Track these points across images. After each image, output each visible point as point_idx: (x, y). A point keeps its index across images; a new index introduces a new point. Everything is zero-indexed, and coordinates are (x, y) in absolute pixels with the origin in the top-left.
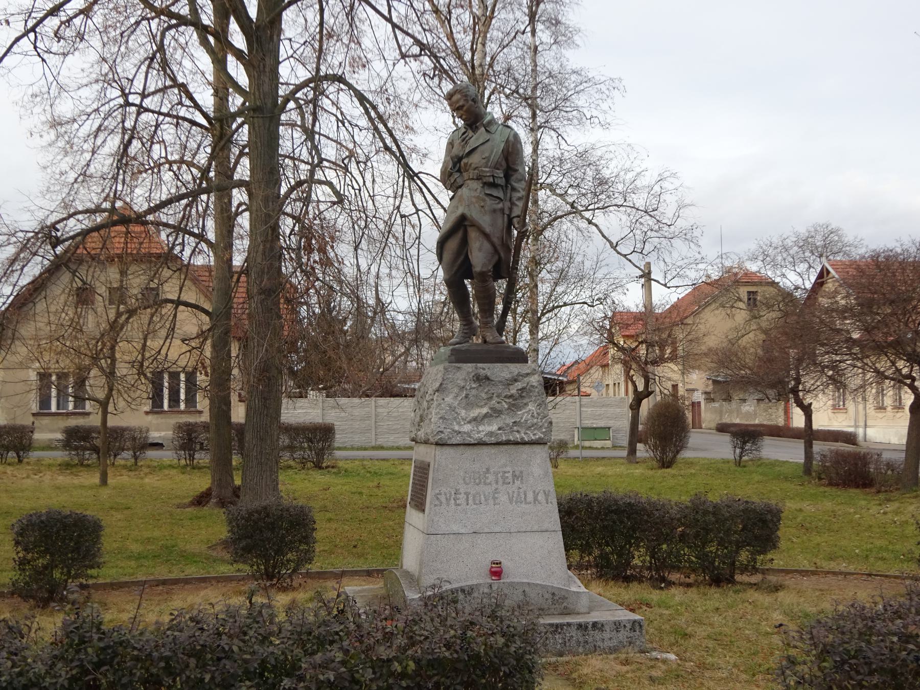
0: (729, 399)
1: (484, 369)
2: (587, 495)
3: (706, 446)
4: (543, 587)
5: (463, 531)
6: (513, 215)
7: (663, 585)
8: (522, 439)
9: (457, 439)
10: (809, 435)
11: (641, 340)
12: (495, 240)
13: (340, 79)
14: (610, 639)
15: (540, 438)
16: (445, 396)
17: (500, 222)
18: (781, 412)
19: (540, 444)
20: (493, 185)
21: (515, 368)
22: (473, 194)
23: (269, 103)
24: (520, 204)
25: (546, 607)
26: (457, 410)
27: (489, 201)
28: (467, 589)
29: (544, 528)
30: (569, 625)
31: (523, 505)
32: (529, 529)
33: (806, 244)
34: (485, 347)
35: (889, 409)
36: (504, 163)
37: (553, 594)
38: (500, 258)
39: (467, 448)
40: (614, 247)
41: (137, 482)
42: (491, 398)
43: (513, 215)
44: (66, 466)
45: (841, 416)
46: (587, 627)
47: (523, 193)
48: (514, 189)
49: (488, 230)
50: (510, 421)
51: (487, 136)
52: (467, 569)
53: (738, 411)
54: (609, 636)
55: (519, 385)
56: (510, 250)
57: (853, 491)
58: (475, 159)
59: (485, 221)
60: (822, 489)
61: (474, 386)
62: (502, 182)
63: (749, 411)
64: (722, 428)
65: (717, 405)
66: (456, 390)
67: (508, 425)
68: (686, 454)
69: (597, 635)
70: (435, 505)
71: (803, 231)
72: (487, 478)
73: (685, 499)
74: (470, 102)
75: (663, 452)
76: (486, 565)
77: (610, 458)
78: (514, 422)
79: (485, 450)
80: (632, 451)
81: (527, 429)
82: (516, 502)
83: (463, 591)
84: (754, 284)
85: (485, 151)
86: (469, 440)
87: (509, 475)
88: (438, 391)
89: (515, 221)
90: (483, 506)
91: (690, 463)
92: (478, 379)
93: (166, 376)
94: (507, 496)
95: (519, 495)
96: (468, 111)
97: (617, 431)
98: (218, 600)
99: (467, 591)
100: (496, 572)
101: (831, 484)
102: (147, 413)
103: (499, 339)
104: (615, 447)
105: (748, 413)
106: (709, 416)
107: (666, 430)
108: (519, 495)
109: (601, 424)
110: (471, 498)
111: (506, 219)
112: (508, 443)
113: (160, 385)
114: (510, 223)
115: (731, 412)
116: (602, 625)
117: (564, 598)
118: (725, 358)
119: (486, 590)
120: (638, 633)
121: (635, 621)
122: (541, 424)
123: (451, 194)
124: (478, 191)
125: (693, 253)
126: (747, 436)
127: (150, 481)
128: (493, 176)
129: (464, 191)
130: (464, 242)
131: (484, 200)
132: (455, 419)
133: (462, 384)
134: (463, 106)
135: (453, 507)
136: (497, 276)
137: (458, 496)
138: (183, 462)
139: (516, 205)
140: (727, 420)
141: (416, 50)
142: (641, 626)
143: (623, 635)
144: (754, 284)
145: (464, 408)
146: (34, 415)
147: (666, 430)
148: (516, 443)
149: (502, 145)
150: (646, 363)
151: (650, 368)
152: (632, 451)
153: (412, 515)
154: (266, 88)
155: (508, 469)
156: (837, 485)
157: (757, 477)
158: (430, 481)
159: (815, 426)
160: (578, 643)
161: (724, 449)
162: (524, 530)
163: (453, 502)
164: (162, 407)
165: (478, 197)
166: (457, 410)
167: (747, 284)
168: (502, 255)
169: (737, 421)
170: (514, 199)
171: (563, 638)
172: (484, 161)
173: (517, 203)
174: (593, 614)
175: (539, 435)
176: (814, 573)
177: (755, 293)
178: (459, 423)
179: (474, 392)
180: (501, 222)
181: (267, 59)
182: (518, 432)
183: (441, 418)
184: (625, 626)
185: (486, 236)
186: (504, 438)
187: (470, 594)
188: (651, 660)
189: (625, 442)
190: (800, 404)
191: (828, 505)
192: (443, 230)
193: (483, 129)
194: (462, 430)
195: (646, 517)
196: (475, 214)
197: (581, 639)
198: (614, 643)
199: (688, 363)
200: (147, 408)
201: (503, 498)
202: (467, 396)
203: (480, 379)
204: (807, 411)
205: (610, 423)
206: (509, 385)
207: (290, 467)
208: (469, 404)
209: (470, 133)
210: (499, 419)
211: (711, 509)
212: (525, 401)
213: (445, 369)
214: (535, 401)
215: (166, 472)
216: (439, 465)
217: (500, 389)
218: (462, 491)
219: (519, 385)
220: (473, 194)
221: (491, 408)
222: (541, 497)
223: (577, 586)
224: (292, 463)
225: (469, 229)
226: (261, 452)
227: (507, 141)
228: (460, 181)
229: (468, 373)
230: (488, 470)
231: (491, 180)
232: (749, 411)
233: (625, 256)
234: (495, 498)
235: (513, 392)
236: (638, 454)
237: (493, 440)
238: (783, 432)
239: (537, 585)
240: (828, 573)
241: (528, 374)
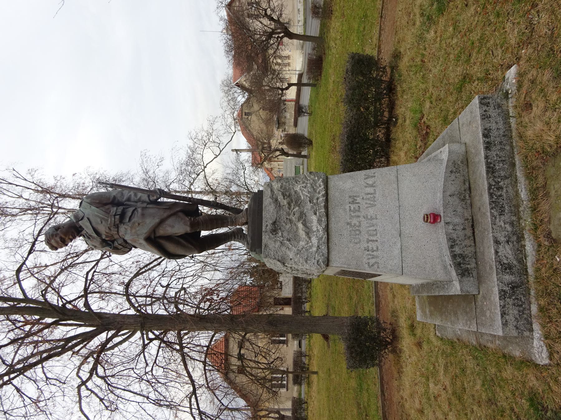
0: (284, 123)
1: (267, 226)
2: (342, 163)
3: (304, 127)
4: (446, 180)
5: (399, 246)
6: (147, 200)
7: (394, 119)
8: (323, 196)
9: (324, 248)
10: (299, 85)
11: (262, 153)
12: (165, 215)
14: (497, 123)
15: (323, 182)
17: (151, 211)
18: (290, 103)
19: (327, 181)
20: (122, 216)
21: (267, 201)
22: (129, 231)
23: (139, 319)
24: (139, 195)
25: (462, 178)
26: (300, 248)
27: (135, 219)
28: (450, 243)
29: (395, 179)
30: (486, 157)
31: (377, 195)
32: (396, 191)
33: (227, 93)
34: (250, 223)
35: (289, 61)
36: (107, 207)
37: (451, 172)
38: (180, 211)
39: (330, 240)
40: (217, 156)
41: (316, 358)
42: (290, 220)
43: (147, 200)
44: (309, 384)
46: (488, 143)
47: (132, 193)
48: (129, 199)
49: (157, 220)
50: (309, 205)
51: (85, 219)
52: (431, 242)
53: (289, 119)
54: (494, 124)
55: (280, 198)
56: (176, 202)
57: (324, 64)
58: (102, 229)
59: (150, 223)
60: (323, 78)
61: (280, 234)
62: (120, 209)
63: (290, 115)
65: (287, 127)
66: (283, 249)
67: (312, 207)
68: (306, 135)
69: (494, 133)
70: (378, 267)
71: (223, 94)
72: (355, 224)
73: (342, 108)
74: (58, 232)
75: (305, 144)
76: (427, 227)
77: (308, 166)
78: (310, 202)
79: (332, 226)
80: (305, 157)
81: (316, 192)
82: (375, 201)
83: (452, 247)
84: (242, 113)
85: (96, 222)
86: (324, 239)
88: (284, 264)
90: (378, 228)
91: (310, 133)
94: (370, 209)
95: (369, 199)
96: (66, 234)
97: (296, 163)
99: (452, 243)
100: (433, 218)
101: (320, 75)
102: (287, 346)
103: (244, 212)
104: (303, 164)
105: (290, 116)
107: (297, 142)
108: (369, 199)
109: (294, 169)
110: (372, 238)
111: (150, 206)
112: (326, 207)
114: (155, 202)
115: (289, 122)
116: (486, 129)
117: (454, 163)
118: (268, 122)
119: (451, 227)
120: (490, 100)
121: (481, 103)
122: (311, 181)
123: (133, 248)
124: (126, 227)
125: (220, 120)
126: (299, 111)
127: (316, 351)
128: (115, 215)
129: (128, 238)
130: (169, 238)
131: (134, 223)
132: (307, 250)
133: (278, 244)
134: (61, 238)
135: (379, 252)
137: (370, 248)
138: (308, 337)
139: (140, 197)
140: (292, 124)
142: (485, 98)
143: (492, 112)
144: (242, 113)
145: (298, 242)
146: (287, 390)
147: (297, 142)
148: (327, 201)
149: (93, 208)
152: (305, 157)
154: (132, 321)
155: (347, 207)
156: (321, 72)
157: (317, 105)
158: (357, 271)
159: (296, 82)
160: (502, 149)
161: (304, 121)
162: (397, 196)
163: (375, 253)
164: (285, 340)
165: (131, 228)
166: (300, 248)
167: (242, 115)
168: (178, 209)
169: (293, 120)
170: (136, 199)
171: (498, 163)
172: (104, 222)
173: (138, 197)
175: (320, 182)
176: (379, 47)
177: (245, 113)
178: (311, 247)
179: (285, 234)
180: (152, 210)
181: (118, 320)
182: (318, 199)
183: (306, 262)
184: (485, 111)
185: (162, 222)
186: (323, 210)
187: (454, 241)
188: (520, 86)
191: (331, 71)
193: (80, 222)
194: (316, 245)
195: (355, 129)
196: (145, 230)
197: (499, 147)
198: (500, 119)
199: (270, 136)
200: (285, 346)
201: (371, 212)
205: (294, 166)
206: (280, 206)
207: (310, 293)
208: (295, 238)
209: (83, 232)
210: (307, 214)
211: (351, 91)
212: (293, 193)
213: (266, 257)
214: (293, 185)
215: (311, 344)
216: (345, 264)
217: (283, 213)
218: (366, 245)
219: (280, 198)
220: (129, 231)
221: (299, 221)
224: (308, 293)
225: (158, 235)
226: (309, 325)
227: (91, 204)
228: (120, 241)
229: (270, 238)
230: (348, 224)
231: (118, 217)
232: (290, 115)
233: (221, 151)
234: (372, 219)
235: (285, 202)
236: (306, 154)
239: (445, 185)
240: (379, 40)
241: (272, 191)
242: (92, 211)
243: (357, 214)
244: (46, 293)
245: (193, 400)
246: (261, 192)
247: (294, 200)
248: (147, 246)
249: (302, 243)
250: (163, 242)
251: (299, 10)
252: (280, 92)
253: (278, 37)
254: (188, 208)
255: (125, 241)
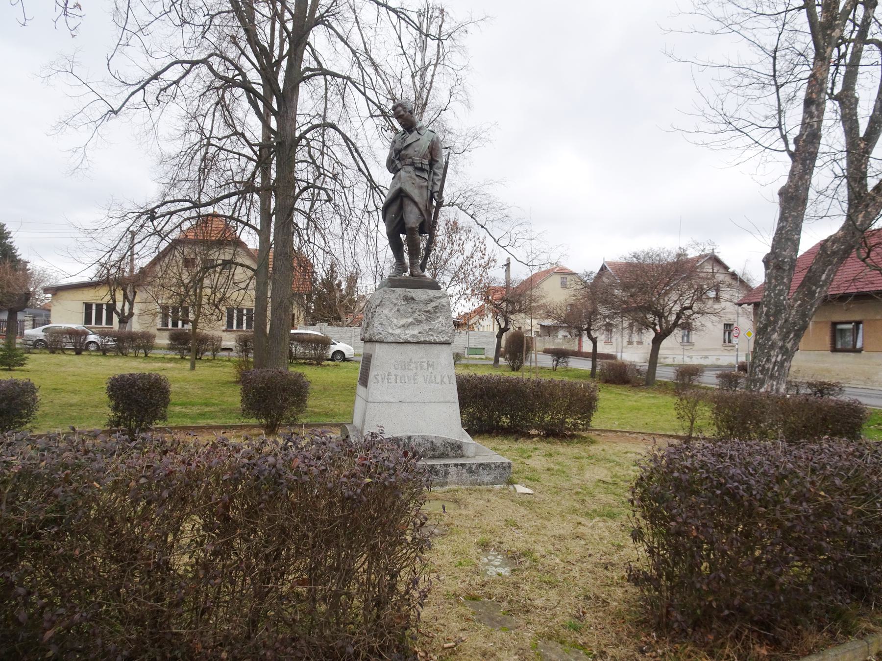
5: (392, 400)
9: (391, 339)
10: (594, 356)
12: (421, 206)
13: (333, 126)
16: (391, 321)
18: (577, 343)
20: (422, 170)
21: (432, 293)
24: (439, 183)
35: (635, 343)
36: (429, 155)
45: (608, 346)
47: (441, 177)
48: (435, 174)
50: (427, 328)
51: (419, 137)
55: (434, 304)
58: (410, 151)
59: (415, 193)
62: (427, 168)
64: (546, 351)
75: (514, 362)
79: (409, 347)
80: (496, 360)
86: (399, 340)
87: (425, 364)
89: (435, 194)
92: (406, 299)
93: (235, 311)
98: (245, 440)
106: (540, 344)
107: (516, 348)
110: (398, 378)
112: (425, 342)
113: (234, 316)
114: (432, 197)
123: (393, 175)
126: (560, 354)
129: (402, 173)
130: (401, 208)
133: (395, 301)
136: (422, 231)
141: (378, 112)
149: (429, 143)
150: (507, 312)
151: (508, 315)
152: (496, 360)
153: (360, 389)
155: (424, 360)
161: (547, 361)
174: (477, 457)
175: (446, 338)
178: (392, 328)
179: (403, 307)
180: (426, 194)
189: (493, 356)
190: (590, 337)
192: (388, 198)
200: (224, 328)
201: (420, 379)
202: (398, 310)
203: (408, 299)
204: (594, 341)
218: (393, 374)
219: (434, 304)
222: (446, 380)
223: (467, 439)
227: (432, 141)
232: (561, 340)
237: (415, 340)
238: (578, 354)
241: (440, 297)
242: (425, 142)
243: (419, 368)
244: (325, 25)
245: (188, 205)
246: (439, 288)
247: (430, 316)
248: (394, 190)
249: (395, 321)
250: (398, 202)
251: (706, 357)
252: (586, 327)
253: (656, 325)
254: (428, 226)
255: (399, 170)
